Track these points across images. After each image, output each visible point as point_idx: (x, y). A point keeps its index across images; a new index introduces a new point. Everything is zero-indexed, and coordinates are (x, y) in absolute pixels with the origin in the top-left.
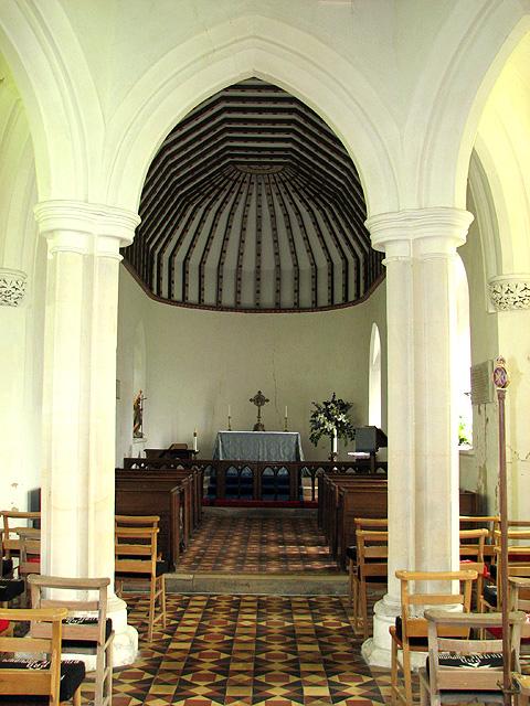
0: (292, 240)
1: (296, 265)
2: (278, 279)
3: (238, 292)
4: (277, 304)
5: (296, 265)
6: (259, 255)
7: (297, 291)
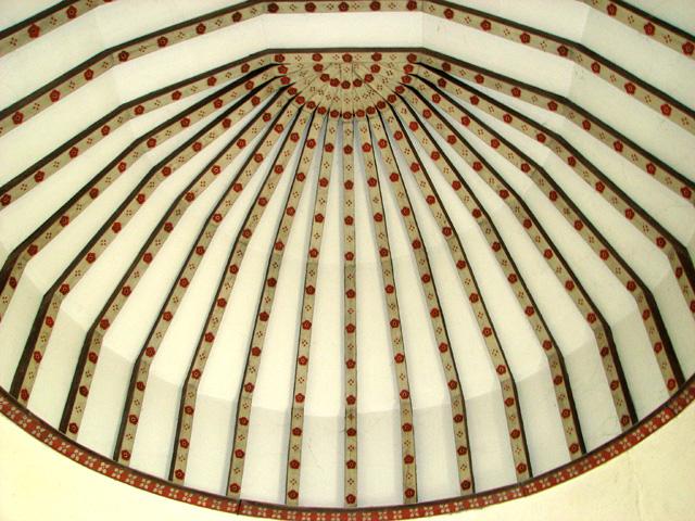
0: (499, 246)
1: (550, 344)
2: (407, 428)
3: (518, 433)
4: (521, 469)
5: (550, 344)
6: (351, 364)
7: (518, 433)
